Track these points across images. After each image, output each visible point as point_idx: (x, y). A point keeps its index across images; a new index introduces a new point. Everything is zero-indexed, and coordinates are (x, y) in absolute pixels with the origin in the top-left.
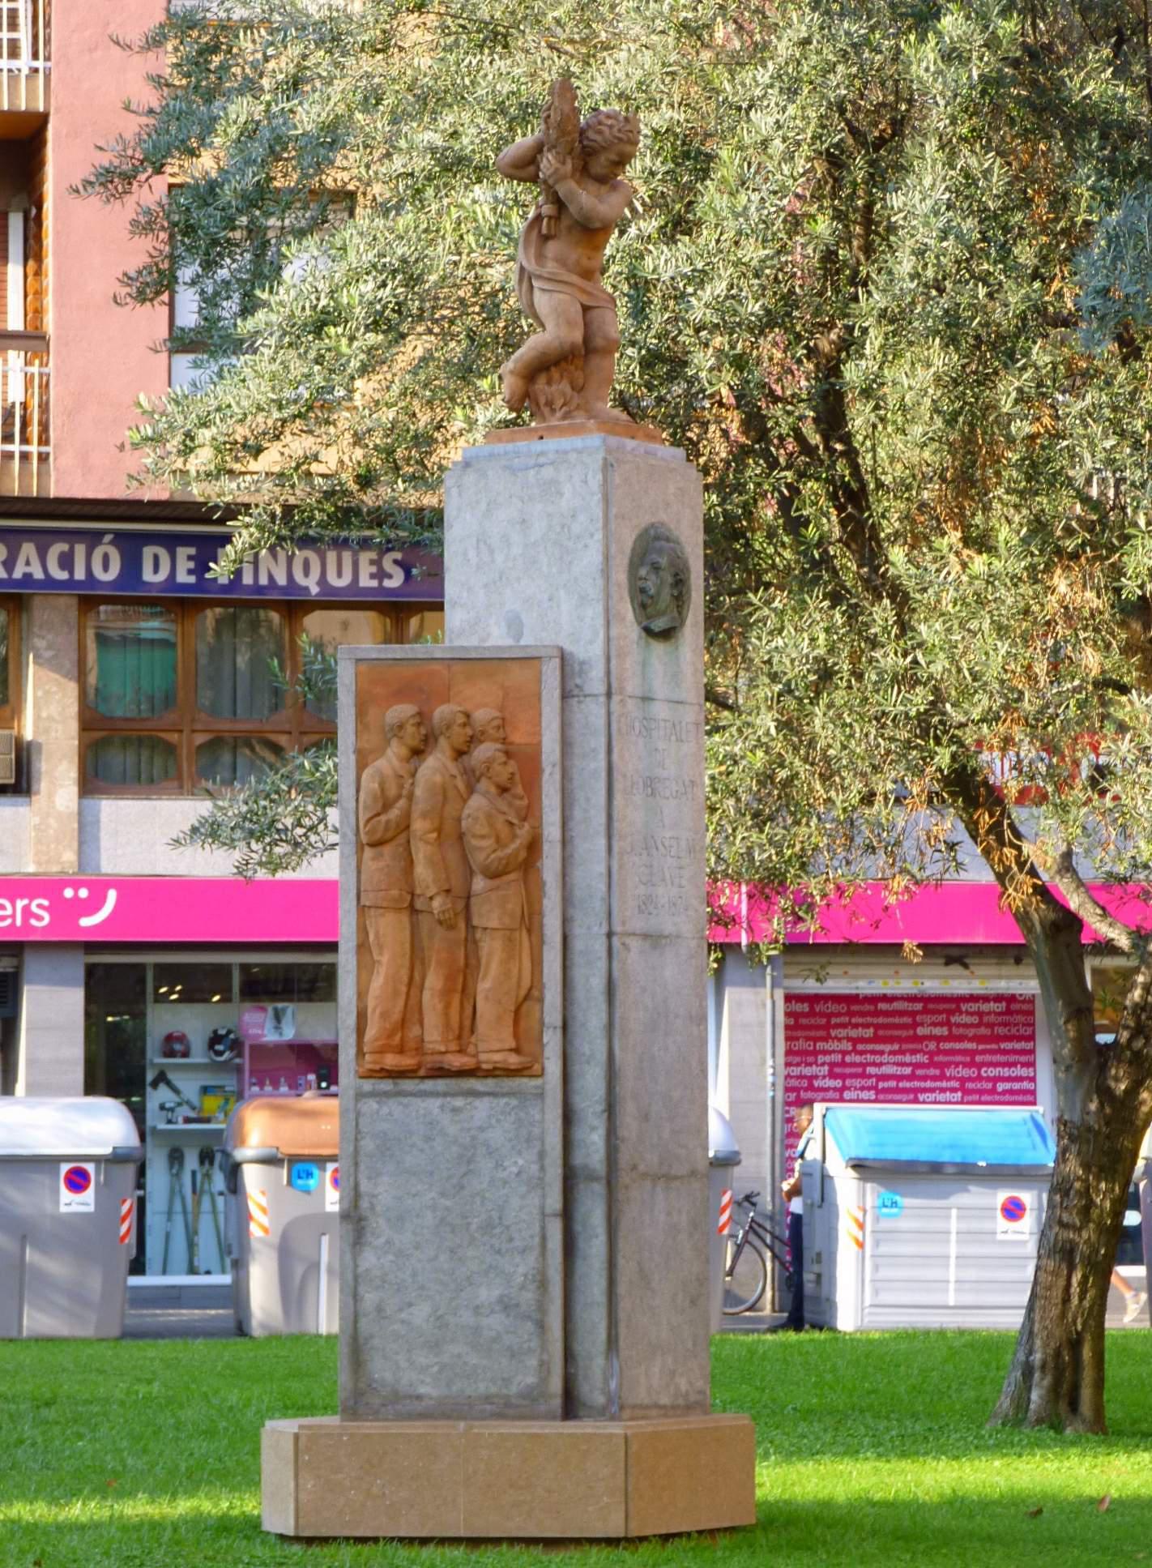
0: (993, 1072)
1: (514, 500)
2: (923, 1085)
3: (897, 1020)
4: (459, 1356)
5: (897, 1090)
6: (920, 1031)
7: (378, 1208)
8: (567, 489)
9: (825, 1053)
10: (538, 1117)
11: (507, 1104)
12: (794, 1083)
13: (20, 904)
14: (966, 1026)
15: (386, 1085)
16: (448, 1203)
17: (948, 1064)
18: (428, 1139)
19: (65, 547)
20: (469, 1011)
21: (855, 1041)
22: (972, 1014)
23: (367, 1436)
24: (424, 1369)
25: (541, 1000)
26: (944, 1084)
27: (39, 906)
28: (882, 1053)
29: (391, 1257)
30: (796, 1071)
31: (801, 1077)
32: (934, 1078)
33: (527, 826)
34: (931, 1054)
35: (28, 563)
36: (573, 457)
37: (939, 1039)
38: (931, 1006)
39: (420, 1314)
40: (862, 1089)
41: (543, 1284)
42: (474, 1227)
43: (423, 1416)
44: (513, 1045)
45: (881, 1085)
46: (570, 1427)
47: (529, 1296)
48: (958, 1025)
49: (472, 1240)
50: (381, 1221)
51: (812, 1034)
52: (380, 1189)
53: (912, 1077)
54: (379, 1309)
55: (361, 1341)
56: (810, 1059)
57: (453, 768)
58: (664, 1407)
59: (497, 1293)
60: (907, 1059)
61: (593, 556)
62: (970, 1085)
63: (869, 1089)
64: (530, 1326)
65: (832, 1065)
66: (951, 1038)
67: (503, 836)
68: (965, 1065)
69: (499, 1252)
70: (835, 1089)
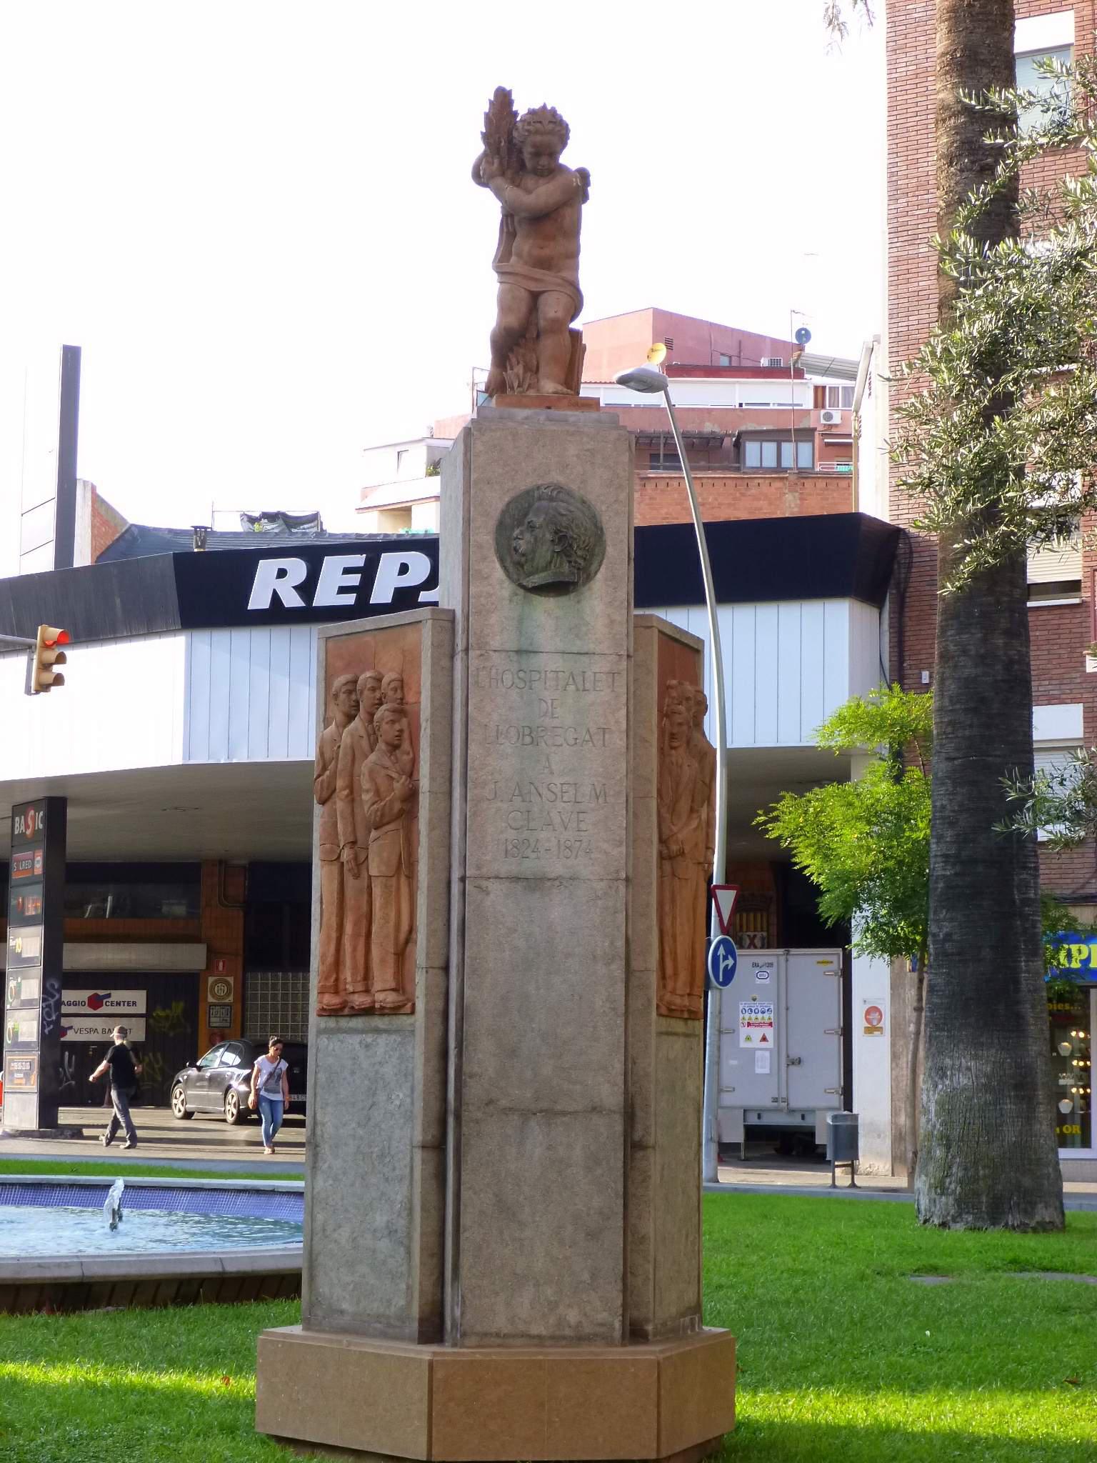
18: (353, 1073)
43: (344, 1330)
44: (393, 985)
50: (327, 1146)
67: (382, 789)
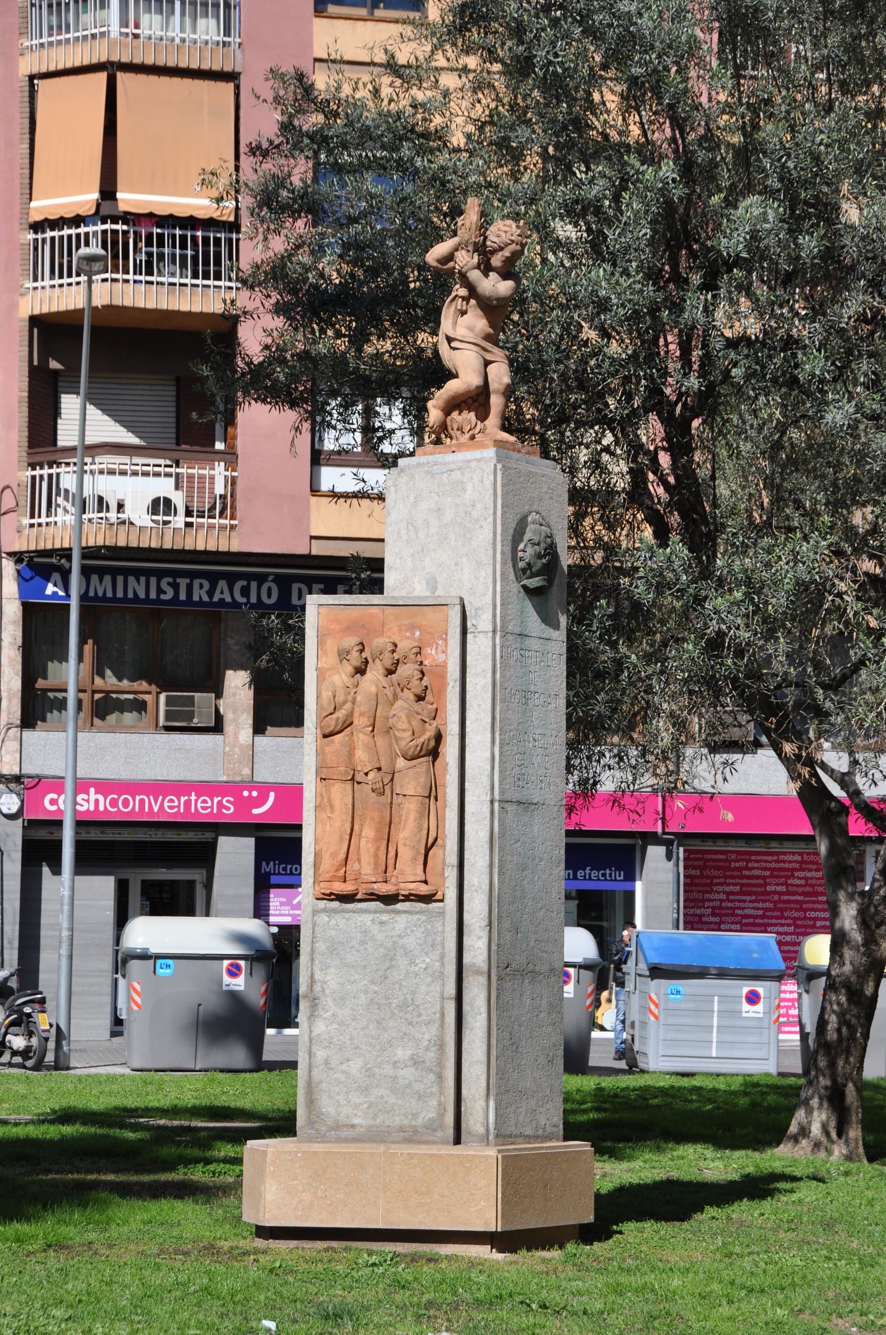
0: (814, 914)
1: (433, 495)
2: (770, 921)
3: (754, 881)
4: (382, 1097)
5: (754, 925)
6: (769, 888)
7: (327, 991)
8: (469, 487)
9: (712, 900)
10: (440, 929)
11: (419, 919)
12: (690, 918)
13: (216, 800)
14: (797, 886)
15: (336, 904)
16: (376, 988)
17: (786, 909)
19: (244, 583)
20: (392, 854)
21: (728, 894)
22: (801, 878)
23: (314, 1153)
24: (356, 1106)
25: (444, 846)
26: (783, 921)
27: (228, 801)
28: (744, 901)
29: (335, 1026)
30: (691, 911)
31: (694, 915)
32: (777, 918)
33: (435, 723)
34: (775, 902)
35: (222, 592)
36: (474, 464)
37: (781, 893)
38: (776, 873)
39: (355, 1067)
40: (732, 923)
41: (442, 1047)
42: (394, 1005)
45: (744, 921)
46: (458, 1150)
47: (432, 1055)
48: (792, 885)
49: (393, 1014)
50: (329, 1000)
51: (702, 889)
52: (328, 978)
53: (763, 917)
54: (327, 1062)
55: (314, 1085)
56: (700, 904)
57: (384, 681)
58: (526, 1136)
59: (409, 1053)
60: (761, 905)
61: (486, 534)
62: (799, 922)
63: (736, 923)
64: (432, 1077)
65: (714, 908)
66: (788, 893)
68: (796, 910)
69: (411, 1023)
70: (715, 923)
